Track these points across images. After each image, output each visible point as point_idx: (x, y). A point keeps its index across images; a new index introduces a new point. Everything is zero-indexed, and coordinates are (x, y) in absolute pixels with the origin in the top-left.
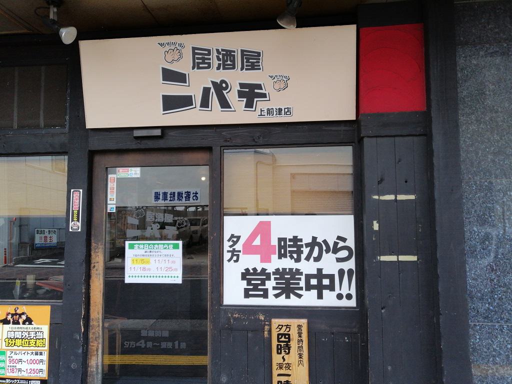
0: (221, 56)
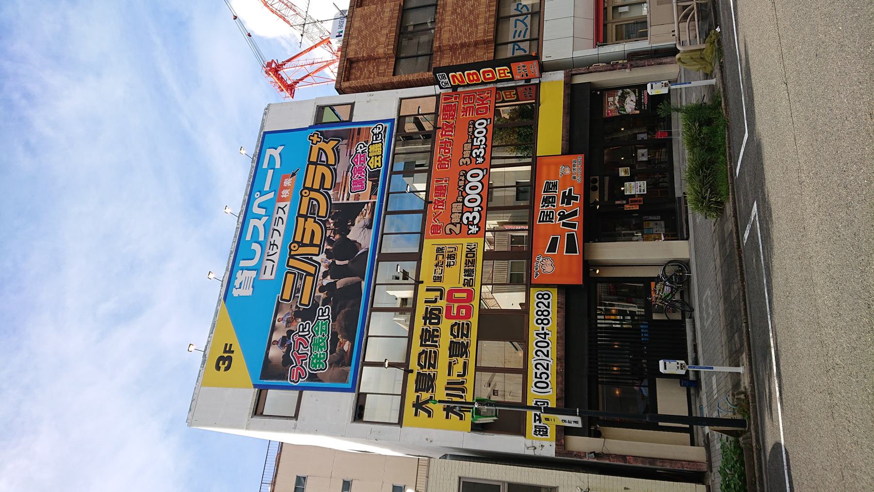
0: (546, 205)
